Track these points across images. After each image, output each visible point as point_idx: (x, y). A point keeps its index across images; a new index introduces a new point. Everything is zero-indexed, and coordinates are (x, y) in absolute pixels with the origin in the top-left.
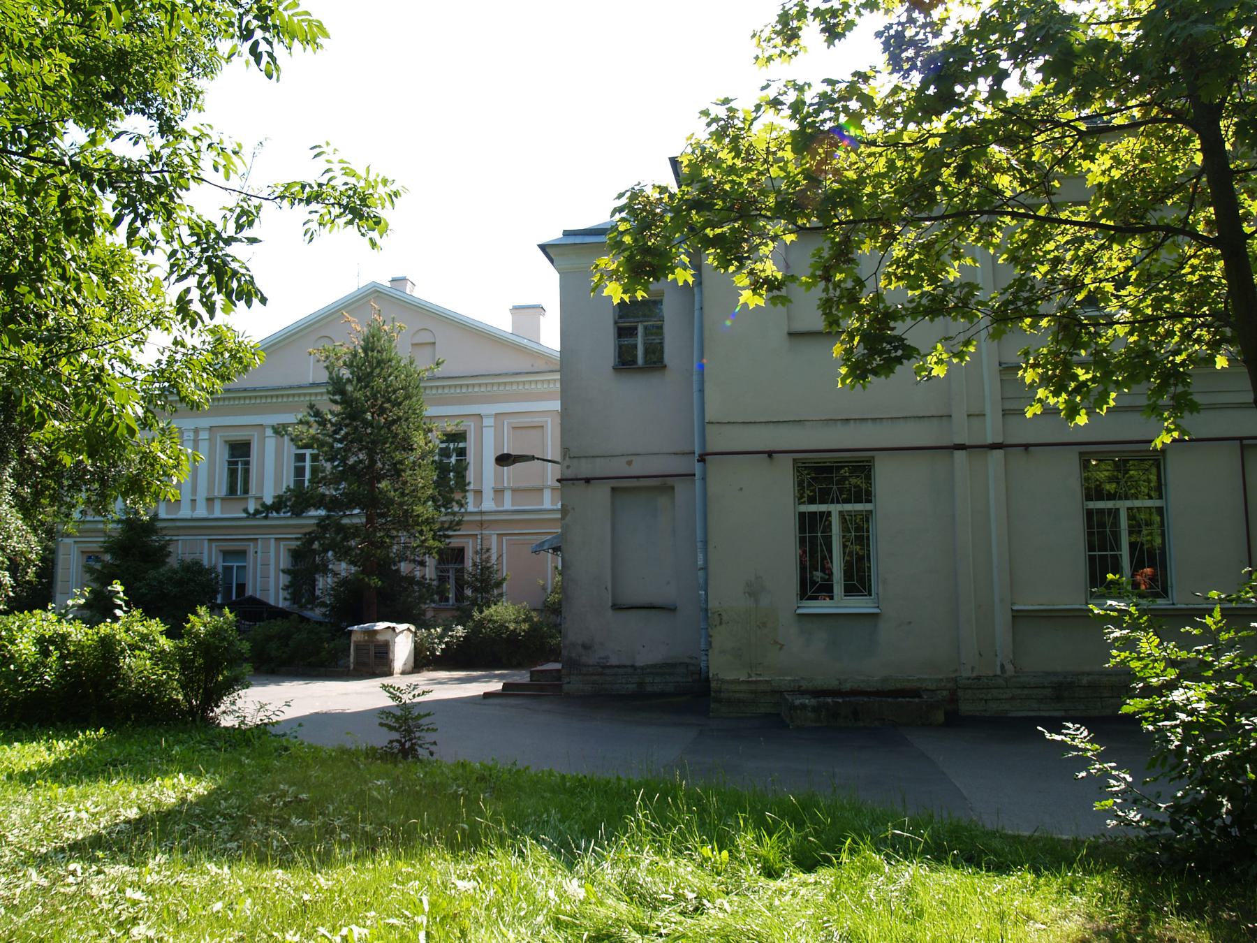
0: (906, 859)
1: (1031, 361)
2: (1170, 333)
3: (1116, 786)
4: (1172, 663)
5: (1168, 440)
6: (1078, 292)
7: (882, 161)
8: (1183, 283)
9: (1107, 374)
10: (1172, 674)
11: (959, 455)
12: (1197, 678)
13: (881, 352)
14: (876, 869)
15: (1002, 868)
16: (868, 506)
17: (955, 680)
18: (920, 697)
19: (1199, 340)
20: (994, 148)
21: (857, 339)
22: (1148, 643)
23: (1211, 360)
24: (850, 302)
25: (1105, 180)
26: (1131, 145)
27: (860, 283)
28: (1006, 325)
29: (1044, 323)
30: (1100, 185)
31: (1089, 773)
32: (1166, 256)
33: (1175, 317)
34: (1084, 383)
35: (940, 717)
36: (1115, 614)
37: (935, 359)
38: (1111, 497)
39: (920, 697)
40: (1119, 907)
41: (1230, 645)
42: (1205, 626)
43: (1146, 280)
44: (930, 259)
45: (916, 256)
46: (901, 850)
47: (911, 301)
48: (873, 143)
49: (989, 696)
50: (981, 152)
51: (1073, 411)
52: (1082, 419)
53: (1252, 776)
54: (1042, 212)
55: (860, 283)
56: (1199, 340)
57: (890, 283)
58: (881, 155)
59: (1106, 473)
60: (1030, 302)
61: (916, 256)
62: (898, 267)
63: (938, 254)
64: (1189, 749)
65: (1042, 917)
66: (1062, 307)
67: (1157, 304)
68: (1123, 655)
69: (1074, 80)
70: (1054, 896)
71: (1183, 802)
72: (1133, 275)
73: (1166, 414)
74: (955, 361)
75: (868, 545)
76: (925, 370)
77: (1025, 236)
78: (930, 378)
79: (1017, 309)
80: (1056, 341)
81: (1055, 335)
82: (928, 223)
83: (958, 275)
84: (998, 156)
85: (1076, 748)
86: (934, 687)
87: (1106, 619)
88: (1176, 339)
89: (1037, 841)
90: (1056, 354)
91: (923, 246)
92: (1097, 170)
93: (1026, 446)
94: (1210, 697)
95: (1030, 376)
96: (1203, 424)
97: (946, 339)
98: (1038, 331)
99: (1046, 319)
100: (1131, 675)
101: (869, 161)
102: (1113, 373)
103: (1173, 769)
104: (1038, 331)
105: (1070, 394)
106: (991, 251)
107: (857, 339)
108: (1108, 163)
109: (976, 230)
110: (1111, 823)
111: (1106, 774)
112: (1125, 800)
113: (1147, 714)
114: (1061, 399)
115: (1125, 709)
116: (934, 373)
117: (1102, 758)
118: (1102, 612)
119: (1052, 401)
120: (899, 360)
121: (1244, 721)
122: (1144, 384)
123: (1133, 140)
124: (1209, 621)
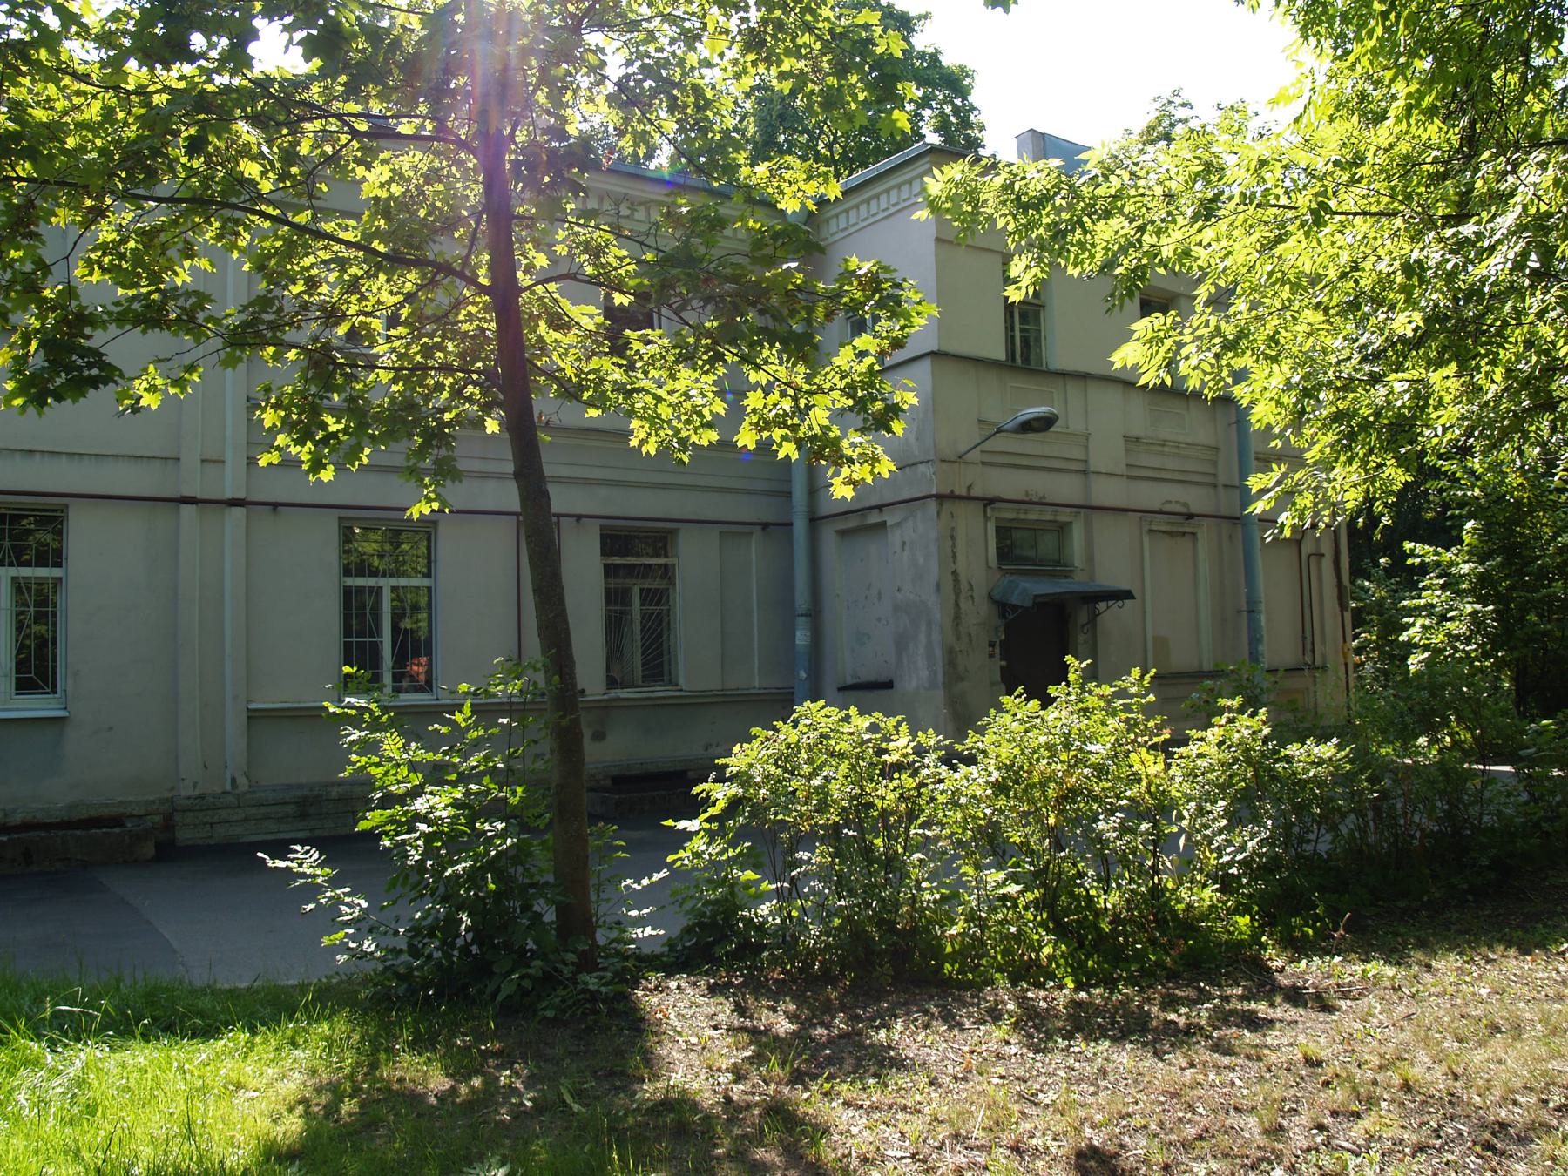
0: (78, 1040)
1: (273, 401)
2: (439, 387)
3: (347, 913)
4: (413, 767)
5: (426, 511)
6: (337, 324)
7: (96, 106)
8: (456, 333)
9: (362, 426)
10: (417, 779)
11: (187, 511)
12: (441, 783)
13: (69, 368)
14: (34, 1063)
15: (208, 1032)
16: (56, 572)
17: (171, 800)
18: (122, 825)
19: (470, 400)
20: (242, 126)
21: (34, 345)
22: (392, 744)
23: (479, 424)
24: (26, 290)
25: (384, 194)
26: (416, 160)
27: (45, 268)
28: (243, 351)
29: (292, 355)
30: (376, 199)
31: (319, 904)
32: (442, 298)
33: (446, 369)
34: (334, 435)
35: (149, 849)
36: (353, 712)
37: (145, 385)
38: (374, 573)
39: (122, 825)
40: (347, 1053)
41: (476, 745)
42: (454, 724)
43: (416, 325)
44: (155, 248)
45: (132, 244)
46: (70, 1030)
47: (118, 304)
48: (85, 78)
49: (216, 819)
50: (226, 120)
51: (317, 465)
52: (327, 475)
53: (492, 887)
54: (303, 218)
55: (45, 268)
56: (470, 400)
57: (91, 274)
58: (94, 96)
59: (374, 546)
60: (274, 326)
61: (132, 244)
62: (104, 254)
63: (164, 248)
64: (429, 863)
65: (254, 1083)
66: (315, 340)
67: (427, 351)
68: (364, 760)
69: (346, 67)
70: (271, 1056)
71: (424, 923)
72: (405, 312)
73: (427, 480)
74: (172, 391)
75: (54, 624)
76: (131, 397)
77: (278, 244)
78: (136, 409)
79: (258, 334)
80: (304, 378)
81: (304, 372)
82: (153, 204)
83: (188, 279)
84: (246, 137)
85: (304, 875)
86: (142, 812)
87: (344, 719)
88: (445, 395)
89: (257, 992)
90: (302, 394)
91: (142, 233)
92: (374, 180)
93: (275, 506)
94: (456, 804)
95: (270, 418)
96: (462, 494)
97: (160, 361)
98: (284, 365)
99: (294, 351)
100: (369, 783)
101: (77, 100)
102: (369, 426)
103: (413, 888)
104: (284, 365)
105: (316, 444)
106: (235, 255)
107: (34, 345)
108: (387, 176)
109: (217, 225)
110: (341, 958)
111: (338, 901)
112: (358, 930)
113: (388, 828)
114: (306, 449)
115: (363, 825)
116: (143, 403)
117: (334, 883)
118: (338, 711)
119: (294, 450)
120: (94, 383)
121: (487, 826)
122: (404, 443)
123: (419, 155)
124: (458, 717)
